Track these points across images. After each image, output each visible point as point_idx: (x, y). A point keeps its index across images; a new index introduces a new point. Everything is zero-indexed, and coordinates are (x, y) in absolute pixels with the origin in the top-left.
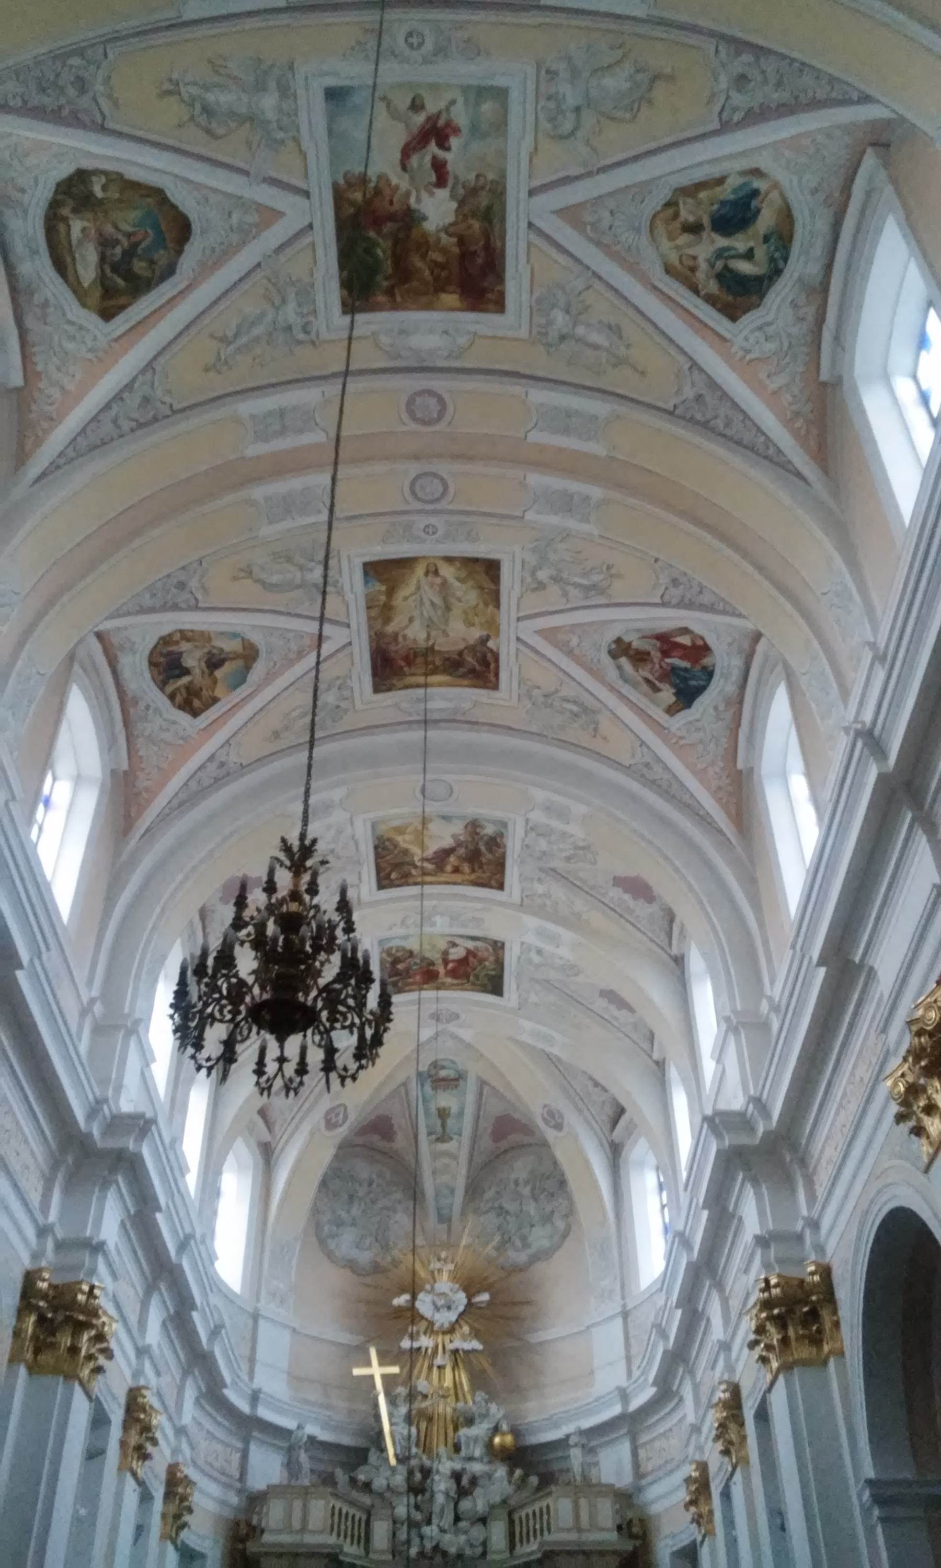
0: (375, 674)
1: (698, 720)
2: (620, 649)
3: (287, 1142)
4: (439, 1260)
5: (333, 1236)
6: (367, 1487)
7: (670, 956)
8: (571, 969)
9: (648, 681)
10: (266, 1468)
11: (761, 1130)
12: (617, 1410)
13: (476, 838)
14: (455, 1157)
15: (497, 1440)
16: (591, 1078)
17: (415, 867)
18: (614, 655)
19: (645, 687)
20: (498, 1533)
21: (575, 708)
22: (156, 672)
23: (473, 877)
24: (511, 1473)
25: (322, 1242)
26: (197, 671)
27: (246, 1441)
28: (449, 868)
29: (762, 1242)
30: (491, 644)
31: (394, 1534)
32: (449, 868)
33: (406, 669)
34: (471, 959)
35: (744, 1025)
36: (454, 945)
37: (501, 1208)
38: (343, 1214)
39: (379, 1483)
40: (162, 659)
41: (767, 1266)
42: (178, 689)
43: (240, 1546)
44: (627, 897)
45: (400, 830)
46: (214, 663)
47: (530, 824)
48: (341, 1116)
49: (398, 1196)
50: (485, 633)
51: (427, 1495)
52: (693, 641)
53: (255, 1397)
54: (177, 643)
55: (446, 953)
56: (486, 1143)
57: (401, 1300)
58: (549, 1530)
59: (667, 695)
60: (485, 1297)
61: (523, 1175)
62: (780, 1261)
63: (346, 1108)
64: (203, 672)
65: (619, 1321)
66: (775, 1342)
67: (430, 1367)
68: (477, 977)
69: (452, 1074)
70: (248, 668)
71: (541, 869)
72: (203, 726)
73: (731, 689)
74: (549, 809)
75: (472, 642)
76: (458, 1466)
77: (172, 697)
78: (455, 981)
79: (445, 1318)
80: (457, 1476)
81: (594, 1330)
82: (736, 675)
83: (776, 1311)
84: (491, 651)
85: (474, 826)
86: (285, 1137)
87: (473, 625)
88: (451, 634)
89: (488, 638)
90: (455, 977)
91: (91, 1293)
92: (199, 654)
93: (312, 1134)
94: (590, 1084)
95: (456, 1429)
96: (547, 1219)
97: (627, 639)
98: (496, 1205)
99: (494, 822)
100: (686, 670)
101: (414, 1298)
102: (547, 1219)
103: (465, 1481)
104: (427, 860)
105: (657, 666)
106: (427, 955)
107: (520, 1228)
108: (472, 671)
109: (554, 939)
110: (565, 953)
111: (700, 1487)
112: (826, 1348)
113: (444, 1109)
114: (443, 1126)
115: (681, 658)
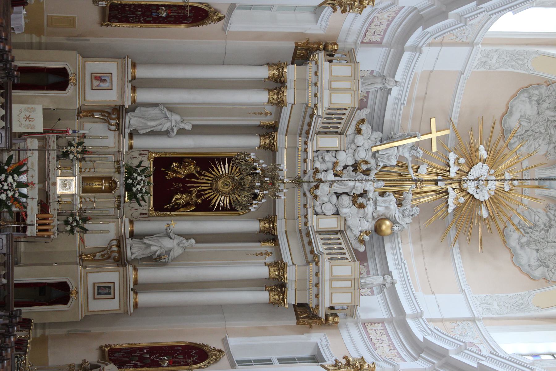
5: (530, 98)
6: (359, 131)
10: (370, 60)
12: (408, 310)
15: (388, 223)
20: (330, 223)
24: (367, 233)
25: (524, 89)
37: (551, 226)
39: (360, 139)
43: (321, 47)
53: (417, 49)
57: (483, 152)
67: (436, 174)
76: (371, 195)
79: (471, 187)
80: (364, 194)
81: (462, 295)
95: (395, 193)
96: (542, 263)
101: (484, 161)
103: (361, 200)
107: (535, 241)
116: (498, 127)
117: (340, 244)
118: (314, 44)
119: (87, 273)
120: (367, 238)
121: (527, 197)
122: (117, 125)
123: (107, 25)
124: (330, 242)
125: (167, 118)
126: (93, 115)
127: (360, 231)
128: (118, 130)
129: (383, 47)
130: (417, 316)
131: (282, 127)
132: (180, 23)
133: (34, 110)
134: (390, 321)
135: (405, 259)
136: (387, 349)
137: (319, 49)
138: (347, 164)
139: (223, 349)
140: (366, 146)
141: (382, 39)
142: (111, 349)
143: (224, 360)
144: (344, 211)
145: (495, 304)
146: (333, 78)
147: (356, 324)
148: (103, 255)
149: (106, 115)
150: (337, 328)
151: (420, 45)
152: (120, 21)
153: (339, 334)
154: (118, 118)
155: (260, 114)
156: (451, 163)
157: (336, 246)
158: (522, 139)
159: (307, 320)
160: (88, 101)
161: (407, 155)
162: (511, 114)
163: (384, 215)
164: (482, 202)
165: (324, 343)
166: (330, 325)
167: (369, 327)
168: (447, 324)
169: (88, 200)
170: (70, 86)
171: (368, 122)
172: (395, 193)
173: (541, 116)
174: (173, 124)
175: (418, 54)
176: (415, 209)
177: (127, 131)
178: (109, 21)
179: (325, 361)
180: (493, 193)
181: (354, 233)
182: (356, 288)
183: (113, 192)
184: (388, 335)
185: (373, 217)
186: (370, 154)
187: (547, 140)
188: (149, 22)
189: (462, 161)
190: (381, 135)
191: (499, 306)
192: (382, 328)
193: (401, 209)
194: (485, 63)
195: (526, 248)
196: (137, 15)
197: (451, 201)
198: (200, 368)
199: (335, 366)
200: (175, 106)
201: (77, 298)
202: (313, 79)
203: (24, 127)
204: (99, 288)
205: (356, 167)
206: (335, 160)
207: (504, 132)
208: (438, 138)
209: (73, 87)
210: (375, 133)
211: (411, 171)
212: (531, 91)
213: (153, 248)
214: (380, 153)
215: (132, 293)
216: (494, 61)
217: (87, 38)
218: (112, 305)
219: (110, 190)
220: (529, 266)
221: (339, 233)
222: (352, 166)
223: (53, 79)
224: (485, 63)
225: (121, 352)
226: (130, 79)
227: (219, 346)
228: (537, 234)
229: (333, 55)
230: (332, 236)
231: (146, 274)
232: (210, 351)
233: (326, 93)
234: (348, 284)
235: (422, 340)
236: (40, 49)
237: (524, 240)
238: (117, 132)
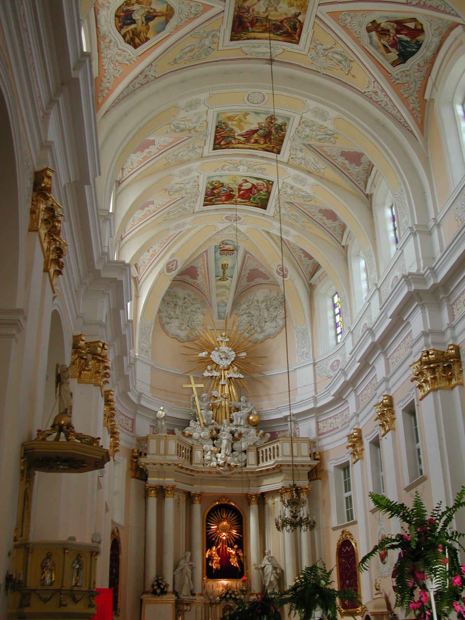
0: (233, 30)
1: (408, 71)
2: (374, 27)
3: (145, 279)
4: (222, 336)
5: (168, 323)
6: (190, 436)
7: (365, 194)
8: (308, 198)
9: (384, 46)
10: (143, 428)
11: (431, 283)
12: (311, 406)
13: (271, 125)
14: (229, 289)
15: (251, 418)
16: (304, 252)
17: (235, 139)
18: (369, 30)
19: (383, 50)
20: (251, 458)
21: (340, 58)
22: (118, 21)
23: (265, 146)
24: (258, 432)
25: (163, 327)
26: (140, 22)
27: (135, 414)
28: (252, 141)
29: (425, 334)
30: (300, 18)
31: (204, 457)
32: (252, 141)
33: (250, 28)
34: (254, 189)
35: (419, 231)
36: (246, 181)
37: (250, 313)
38: (172, 314)
39: (196, 435)
40: (122, 14)
41: (426, 345)
42: (128, 31)
43: (135, 460)
44: (346, 162)
45: (230, 118)
46: (149, 17)
47: (303, 120)
48: (174, 267)
49: (198, 306)
50: (298, 11)
51: (219, 441)
52: (416, 26)
53: (140, 396)
54: (133, 4)
55: (241, 185)
56: (244, 282)
57: (204, 354)
58: (278, 456)
59: (394, 55)
60: (244, 354)
61: (261, 298)
62: (433, 343)
63: (177, 262)
64: (143, 23)
65: (311, 367)
66: (429, 379)
67: (218, 385)
68: (254, 199)
69: (231, 247)
70: (167, 22)
71: (304, 145)
72: (139, 54)
73: (429, 54)
74: (316, 112)
75: (290, 16)
76: (234, 429)
77: (124, 36)
78: (242, 201)
79: (225, 363)
80: (232, 433)
81: (298, 371)
82: (433, 47)
83: (432, 365)
84: (299, 21)
85: (272, 119)
86: (145, 276)
87: (293, 6)
88: (279, 10)
89: (300, 14)
90: (242, 199)
91: (103, 348)
92: (142, 12)
93: (160, 274)
94: (303, 255)
95: (230, 413)
96: (274, 319)
97: (378, 22)
98: (247, 312)
99: (283, 117)
100: (407, 42)
101: (210, 353)
102: (274, 319)
103: (236, 435)
104: (241, 135)
105: (391, 38)
106: (231, 186)
107: (259, 323)
108: (287, 32)
109: (302, 182)
110: (308, 189)
111: (356, 440)
112: (454, 382)
113: (225, 265)
114: (224, 273)
115: (406, 35)
116: (186, 344)
117: (266, 450)
118: (132, 465)
120: (261, 432)
121: (232, 327)
122: (187, 604)
124: (265, 457)
125: (182, 570)
128: (190, 604)
130: (315, 400)
131: (188, 488)
135: (274, 407)
136: (337, 420)
137: (136, 462)
139: (342, 530)
141: (131, 419)
143: (349, 529)
144: (244, 446)
145: (303, 350)
146: (158, 453)
147: (319, 440)
150: (323, 452)
153: (328, 451)
154: (183, 604)
155: (179, 503)
156: (210, 375)
157: (268, 453)
158: (193, 329)
159: (318, 473)
161: (206, 404)
162: (178, 335)
163: (245, 420)
165: (334, 461)
166: (321, 456)
167: (321, 431)
168: (317, 381)
172: (230, 413)
173: (179, 317)
174: (186, 564)
176: (242, 400)
177: (191, 597)
179: (348, 462)
184: (327, 419)
185: (248, 427)
187: (194, 313)
188: (118, 581)
189: (209, 367)
190: (192, 421)
193: (242, 409)
194: (146, 351)
198: (356, 546)
199: (354, 455)
202: (158, 466)
205: (214, 438)
206: (209, 453)
207: (189, 340)
208: (195, 383)
210: (191, 425)
211: (216, 401)
212: (164, 322)
213: (272, 579)
214: (205, 421)
216: (145, 345)
222: (213, 440)
224: (146, 351)
227: (339, 532)
228: (254, 322)
229: (141, 453)
230: (261, 455)
232: (343, 538)
233: (168, 458)
234: (295, 445)
235: (333, 397)
237: (259, 330)
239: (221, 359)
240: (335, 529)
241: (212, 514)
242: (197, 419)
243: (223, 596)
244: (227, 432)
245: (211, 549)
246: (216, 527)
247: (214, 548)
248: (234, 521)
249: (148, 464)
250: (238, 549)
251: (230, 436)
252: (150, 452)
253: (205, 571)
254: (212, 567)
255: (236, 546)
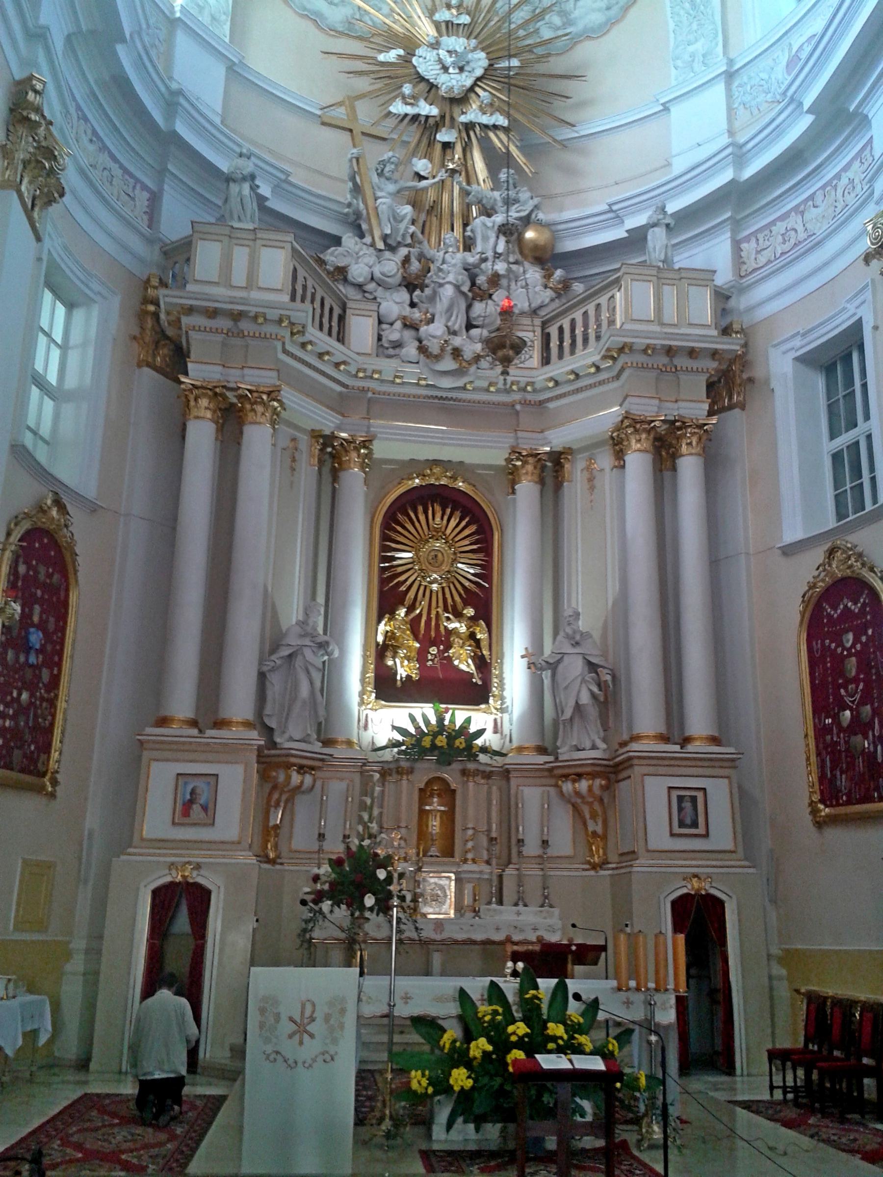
6: (341, 273)
12: (727, 175)
24: (548, 276)
27: (161, 173)
39: (358, 272)
51: (428, 291)
53: (174, 100)
57: (392, 56)
65: (720, 88)
81: (674, 109)
103: (481, 280)
119: (648, 851)
122: (302, 769)
123: (55, 782)
126: (276, 827)
127: (546, 287)
129: (161, 190)
132: (65, 604)
133: (269, 1005)
134: (736, 224)
135: (590, 206)
136: (812, 213)
138: (408, 302)
139: (827, 546)
140: (372, 260)
141: (145, 187)
142: (822, 801)
145: (691, 49)
147: (743, 290)
148: (594, 816)
149: (276, 796)
151: (163, 89)
152: (47, 748)
156: (410, 110)
160: (243, 829)
162: (319, 14)
164: (491, 65)
165: (797, 342)
167: (751, 265)
168: (737, 124)
169: (470, 845)
170: (200, 880)
171: (322, 252)
175: (182, 101)
178: (44, 775)
180: (473, 42)
181: (547, 300)
182: (677, 277)
183: (453, 786)
184: (773, 223)
186: (387, 254)
191: (696, 40)
192: (753, 240)
195: (573, 16)
196: (31, 704)
197: (485, 119)
200: (268, 635)
201: (709, 876)
203: (335, 1041)
204: (682, 824)
205: (411, 285)
206: (398, 325)
209: (202, 872)
213: (585, 698)
215: (690, 748)
217: (86, 833)
218: (719, 794)
219: (449, 794)
220: (608, 8)
221: (547, 331)
222: (411, 293)
223: (182, 923)
225: (834, 776)
226: (195, 732)
231: (646, 714)
236: (99, 952)
238: (319, 774)
239: (445, 69)
240: (788, 551)
241: (400, 517)
242: (364, 226)
243: (427, 742)
244: (454, 265)
245: (392, 617)
246: (410, 555)
247: (402, 612)
248: (467, 542)
249: (190, 310)
250: (473, 619)
251: (464, 280)
252: (197, 277)
253: (371, 675)
254: (393, 672)
255: (470, 612)
